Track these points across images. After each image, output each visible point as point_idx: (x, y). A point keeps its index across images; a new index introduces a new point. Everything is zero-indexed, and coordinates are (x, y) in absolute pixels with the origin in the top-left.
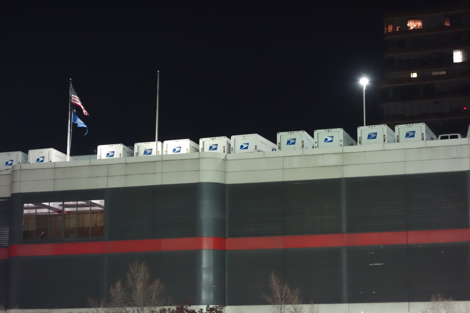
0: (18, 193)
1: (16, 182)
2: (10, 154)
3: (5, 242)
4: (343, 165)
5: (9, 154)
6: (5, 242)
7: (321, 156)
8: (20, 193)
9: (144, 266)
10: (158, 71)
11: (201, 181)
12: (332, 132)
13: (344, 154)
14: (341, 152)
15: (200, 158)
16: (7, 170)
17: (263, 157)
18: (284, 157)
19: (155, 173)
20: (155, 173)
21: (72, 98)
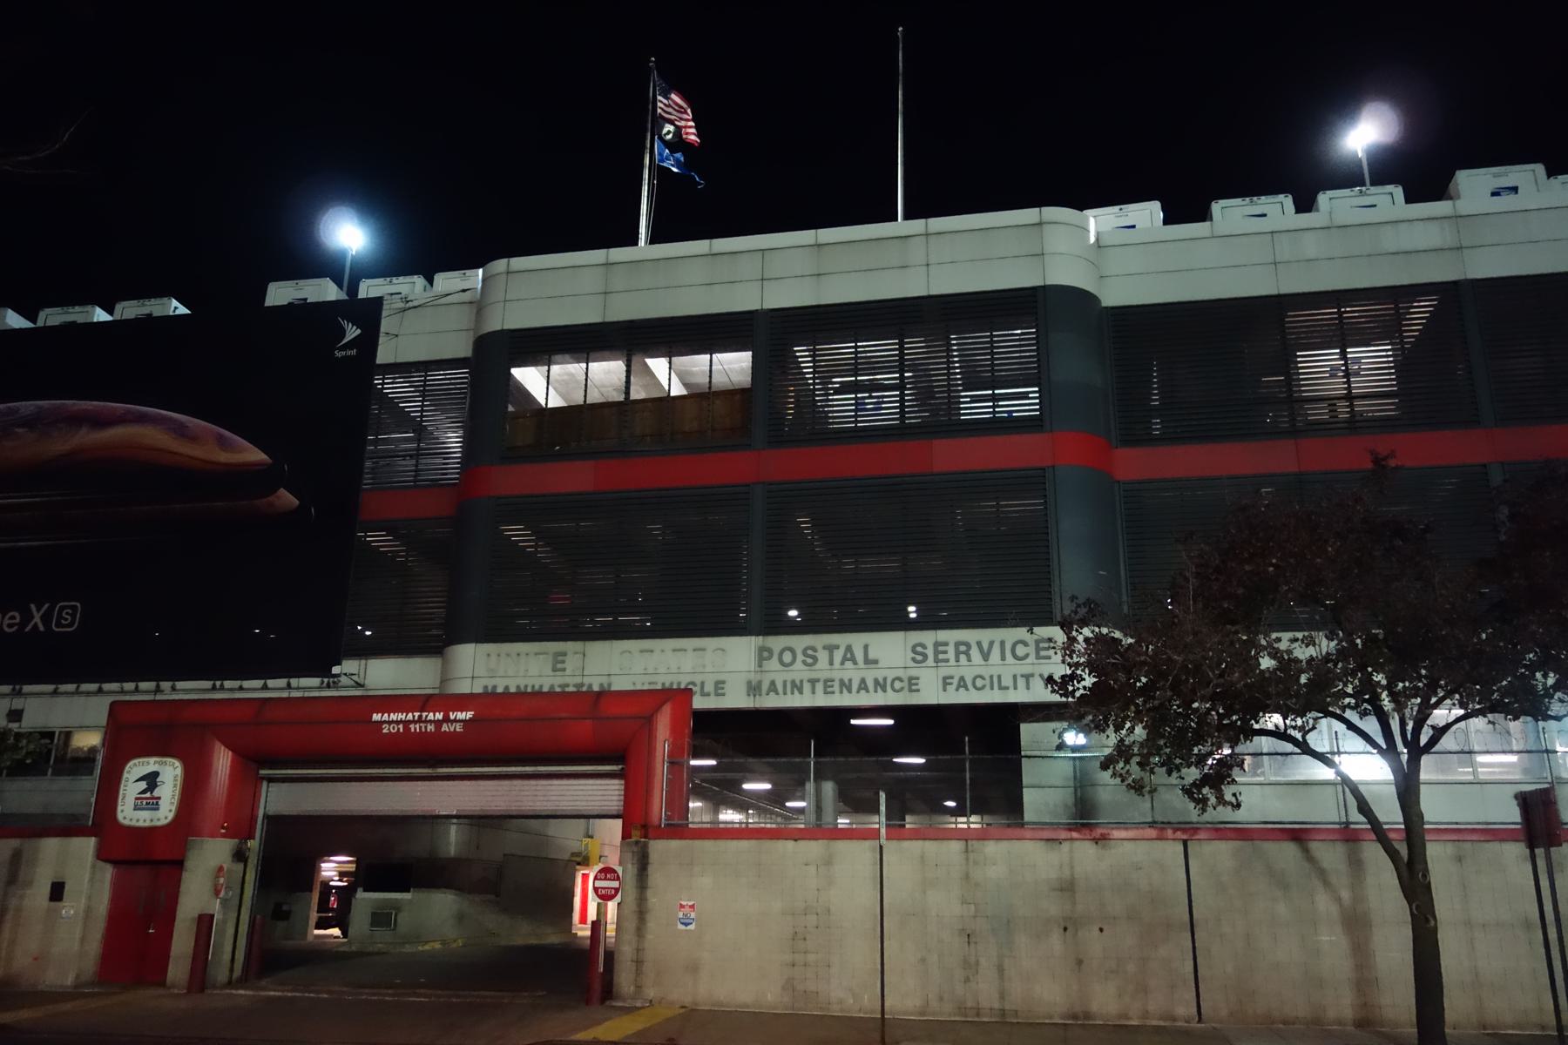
0: (498, 331)
1: (494, 303)
2: (467, 275)
3: (452, 474)
4: (1461, 248)
5: (464, 274)
6: (452, 474)
7: (1389, 227)
8: (502, 331)
9: (1361, 167)
10: (900, 29)
11: (1049, 282)
12: (1369, 195)
13: (1459, 219)
14: (1451, 215)
15: (1045, 223)
16: (464, 291)
17: (1208, 235)
18: (1272, 232)
19: (907, 267)
20: (907, 267)
21: (659, 104)
